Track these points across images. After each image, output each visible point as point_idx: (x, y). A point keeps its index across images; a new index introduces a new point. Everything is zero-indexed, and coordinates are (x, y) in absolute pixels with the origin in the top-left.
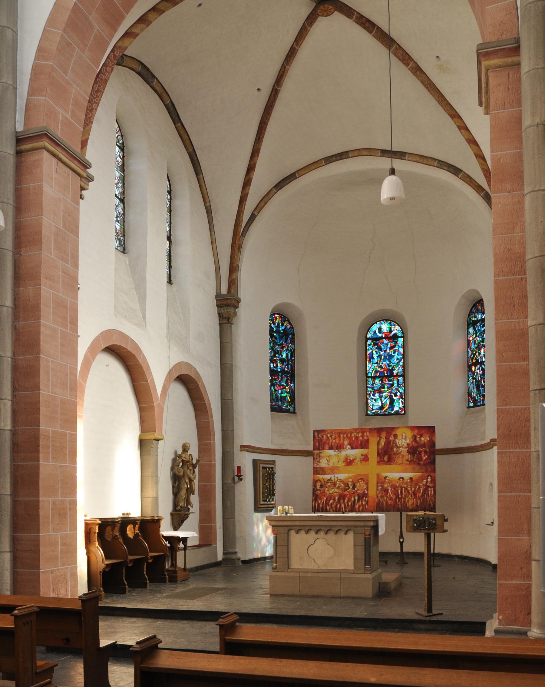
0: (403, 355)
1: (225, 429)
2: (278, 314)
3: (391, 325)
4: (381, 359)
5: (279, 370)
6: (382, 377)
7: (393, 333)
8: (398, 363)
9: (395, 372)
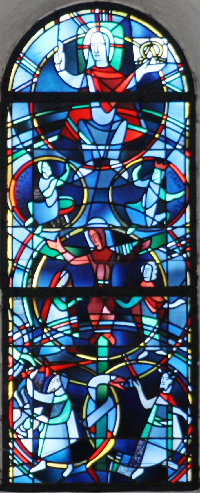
3: (128, 32)
4: (78, 204)
7: (140, 73)
9: (149, 272)
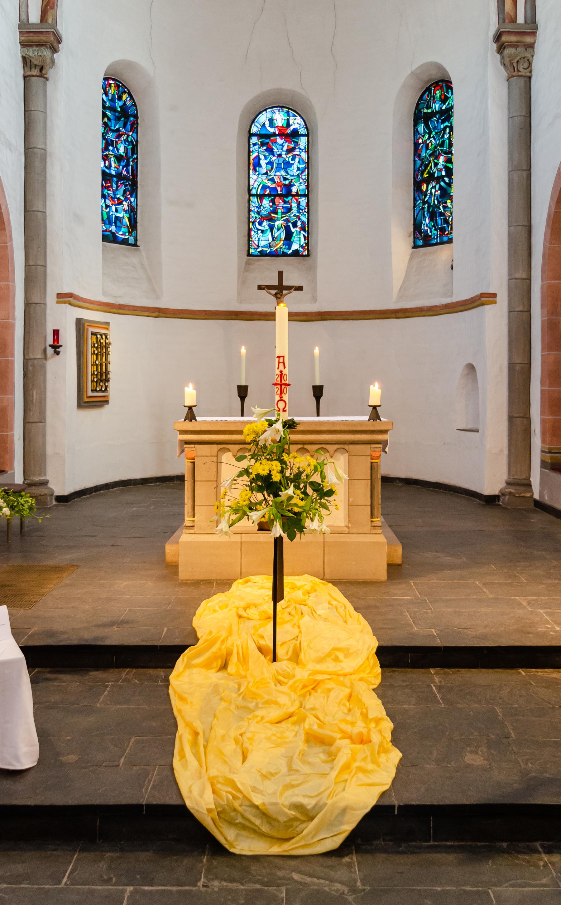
0: (308, 163)
1: (31, 263)
2: (113, 80)
3: (288, 115)
5: (113, 173)
6: (273, 195)
7: (292, 128)
8: (298, 175)
9: (294, 190)
